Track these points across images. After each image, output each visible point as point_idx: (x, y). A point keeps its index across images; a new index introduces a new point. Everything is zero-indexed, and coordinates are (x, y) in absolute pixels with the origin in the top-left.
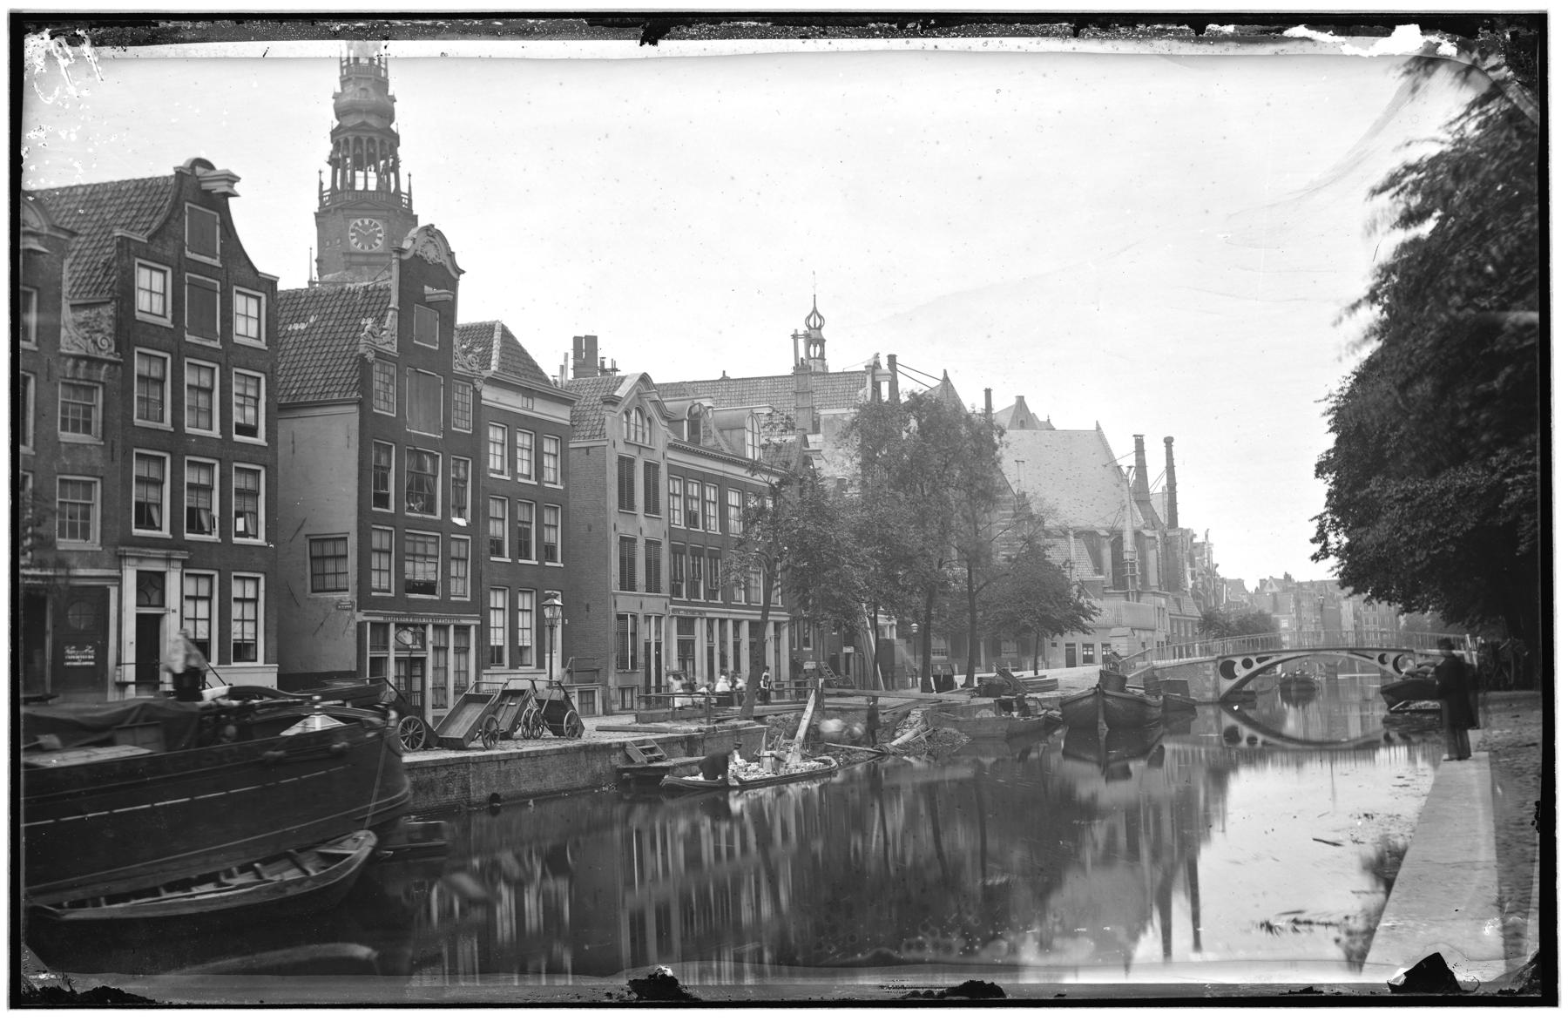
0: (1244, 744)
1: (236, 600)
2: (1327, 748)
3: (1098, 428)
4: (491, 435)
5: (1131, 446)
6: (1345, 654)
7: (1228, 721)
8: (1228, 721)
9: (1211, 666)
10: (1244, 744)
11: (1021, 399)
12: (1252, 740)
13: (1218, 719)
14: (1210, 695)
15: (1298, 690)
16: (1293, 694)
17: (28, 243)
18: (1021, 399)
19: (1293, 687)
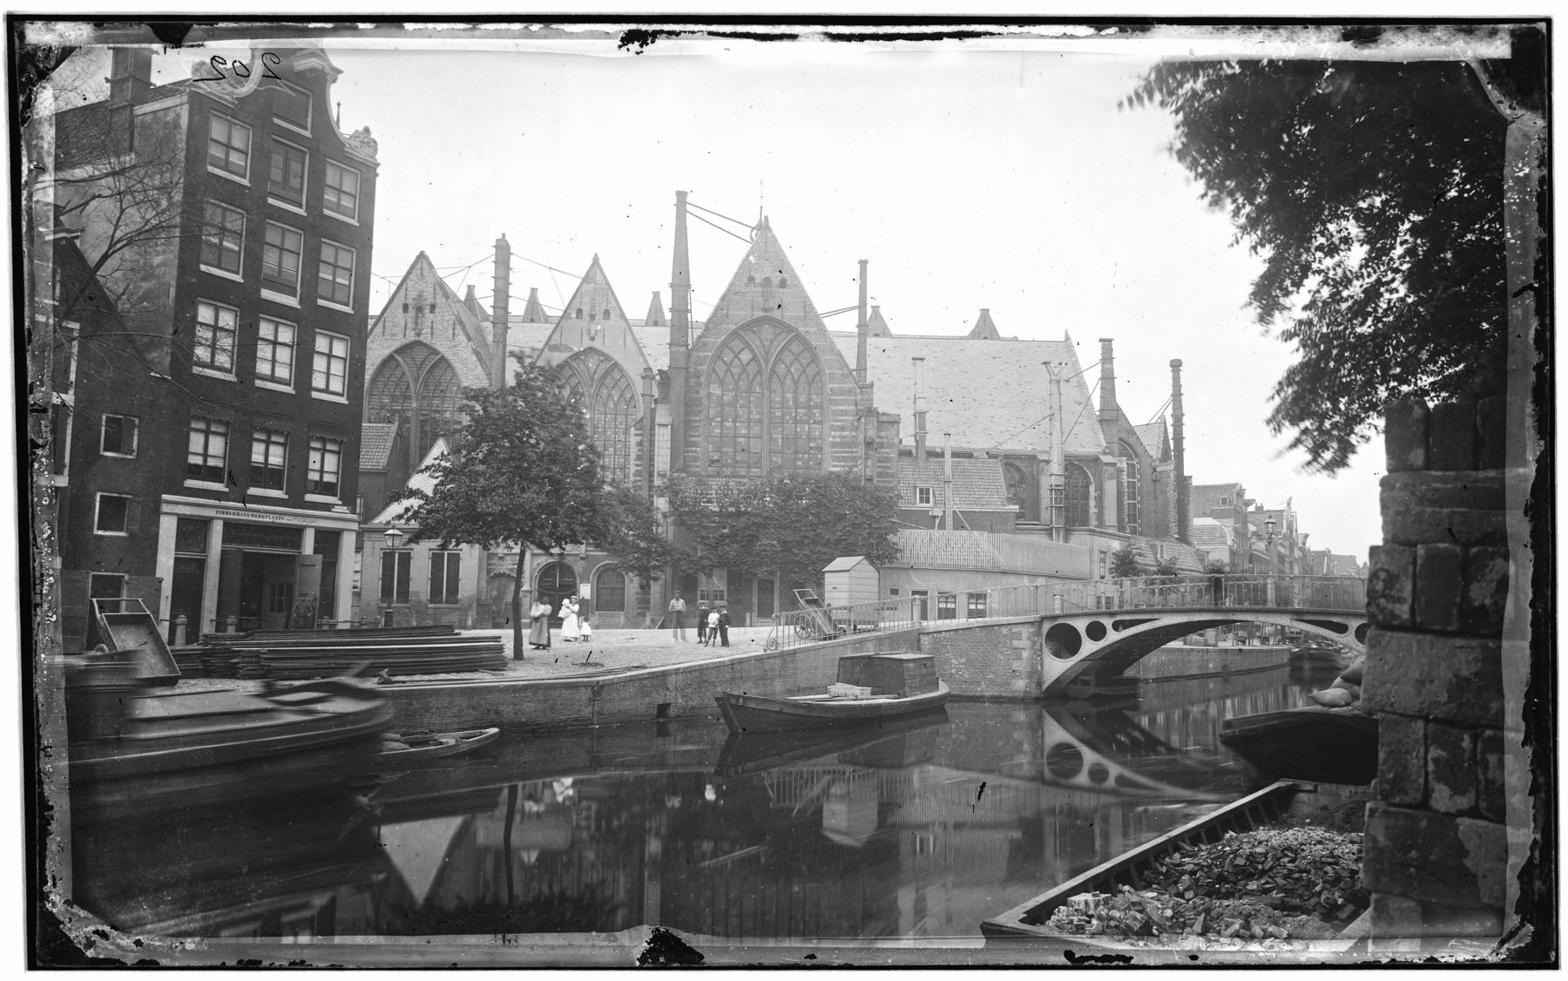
0: (1083, 778)
1: (205, 461)
2: (676, 671)
3: (1068, 338)
4: (209, 211)
5: (1097, 353)
6: (1026, 581)
7: (1056, 734)
8: (1056, 734)
9: (1026, 632)
10: (1083, 778)
11: (985, 313)
12: (1098, 774)
13: (1036, 728)
14: (1020, 685)
15: (1313, 669)
16: (1307, 674)
17: (286, 964)
18: (985, 313)
19: (1307, 665)
